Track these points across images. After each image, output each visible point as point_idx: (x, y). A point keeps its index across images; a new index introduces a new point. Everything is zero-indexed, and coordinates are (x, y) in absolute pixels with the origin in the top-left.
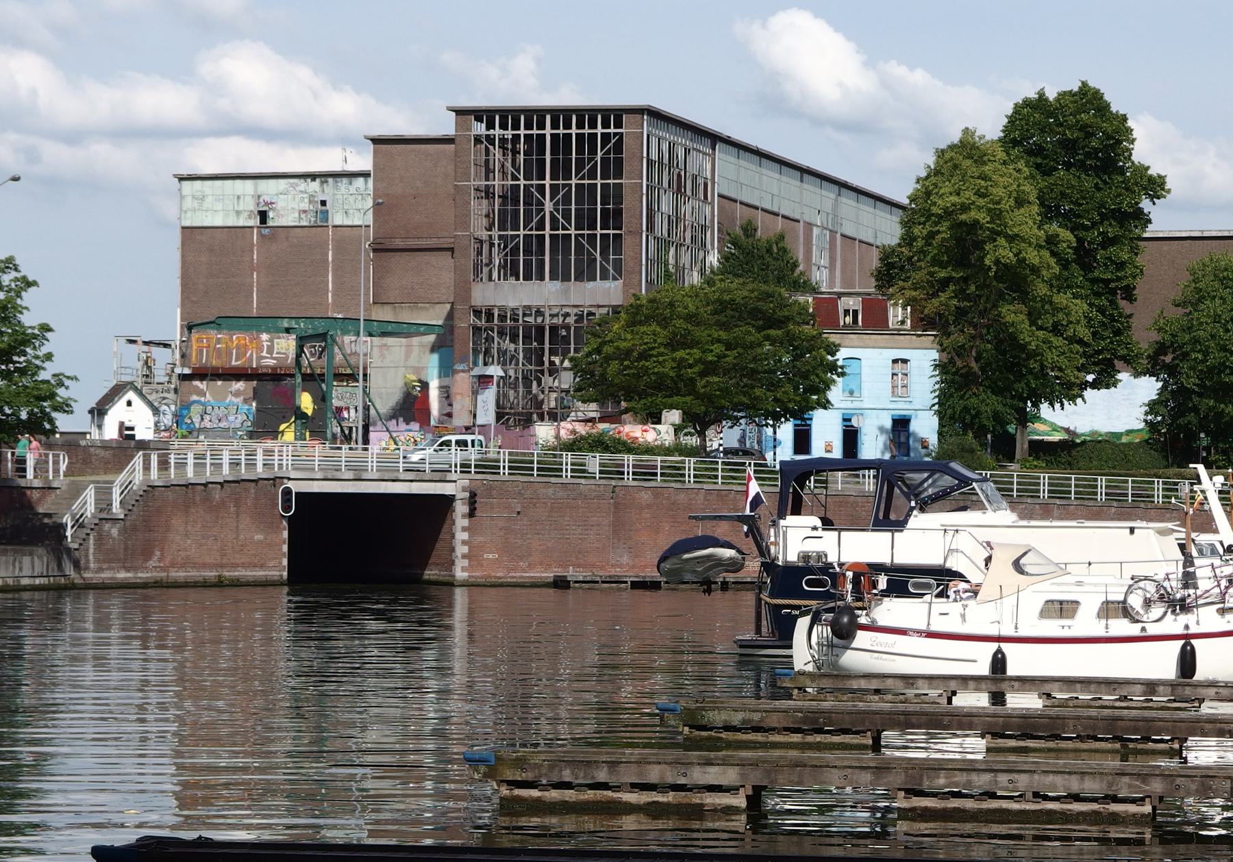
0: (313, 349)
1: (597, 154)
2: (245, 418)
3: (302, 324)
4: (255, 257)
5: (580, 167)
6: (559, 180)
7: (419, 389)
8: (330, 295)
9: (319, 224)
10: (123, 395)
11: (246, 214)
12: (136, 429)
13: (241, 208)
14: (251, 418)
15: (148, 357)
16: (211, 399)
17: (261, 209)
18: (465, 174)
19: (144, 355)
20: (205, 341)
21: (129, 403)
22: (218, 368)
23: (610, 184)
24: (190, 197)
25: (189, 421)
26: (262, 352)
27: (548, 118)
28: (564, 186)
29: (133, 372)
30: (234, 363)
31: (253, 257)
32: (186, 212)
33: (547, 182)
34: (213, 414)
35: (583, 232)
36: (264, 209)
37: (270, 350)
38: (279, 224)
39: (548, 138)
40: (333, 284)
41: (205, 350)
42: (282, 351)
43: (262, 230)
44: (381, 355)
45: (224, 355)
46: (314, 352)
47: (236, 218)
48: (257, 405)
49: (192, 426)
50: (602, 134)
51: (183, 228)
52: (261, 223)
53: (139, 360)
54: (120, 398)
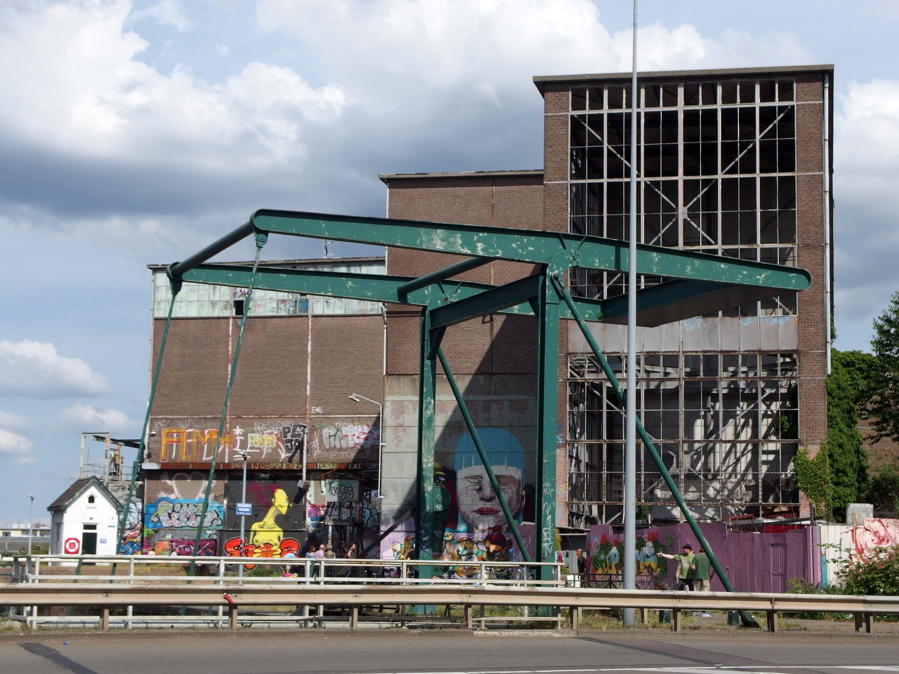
0: (289, 444)
1: (755, 138)
2: (215, 516)
3: (480, 246)
4: (230, 348)
5: (729, 152)
6: (698, 174)
7: (443, 479)
8: (308, 387)
9: (298, 313)
10: (85, 490)
11: (222, 304)
12: (98, 527)
13: (217, 298)
14: (221, 516)
15: (115, 455)
16: (180, 496)
17: (237, 299)
18: (559, 170)
19: (113, 453)
20: (175, 435)
21: (91, 499)
22: (188, 464)
23: (775, 178)
24: (165, 288)
25: (156, 520)
26: (235, 447)
27: (681, 91)
28: (706, 183)
29: (103, 469)
30: (205, 459)
31: (228, 348)
32: (159, 303)
33: (680, 178)
34: (181, 512)
35: (735, 247)
36: (241, 299)
37: (244, 445)
38: (256, 315)
39: (681, 117)
40: (311, 375)
41: (175, 444)
42: (256, 446)
43: (238, 320)
44: (396, 438)
45: (195, 450)
46: (290, 447)
47: (210, 308)
48: (228, 502)
49: (159, 525)
50: (761, 108)
51: (156, 319)
52: (236, 314)
53: (106, 457)
54: (81, 494)
